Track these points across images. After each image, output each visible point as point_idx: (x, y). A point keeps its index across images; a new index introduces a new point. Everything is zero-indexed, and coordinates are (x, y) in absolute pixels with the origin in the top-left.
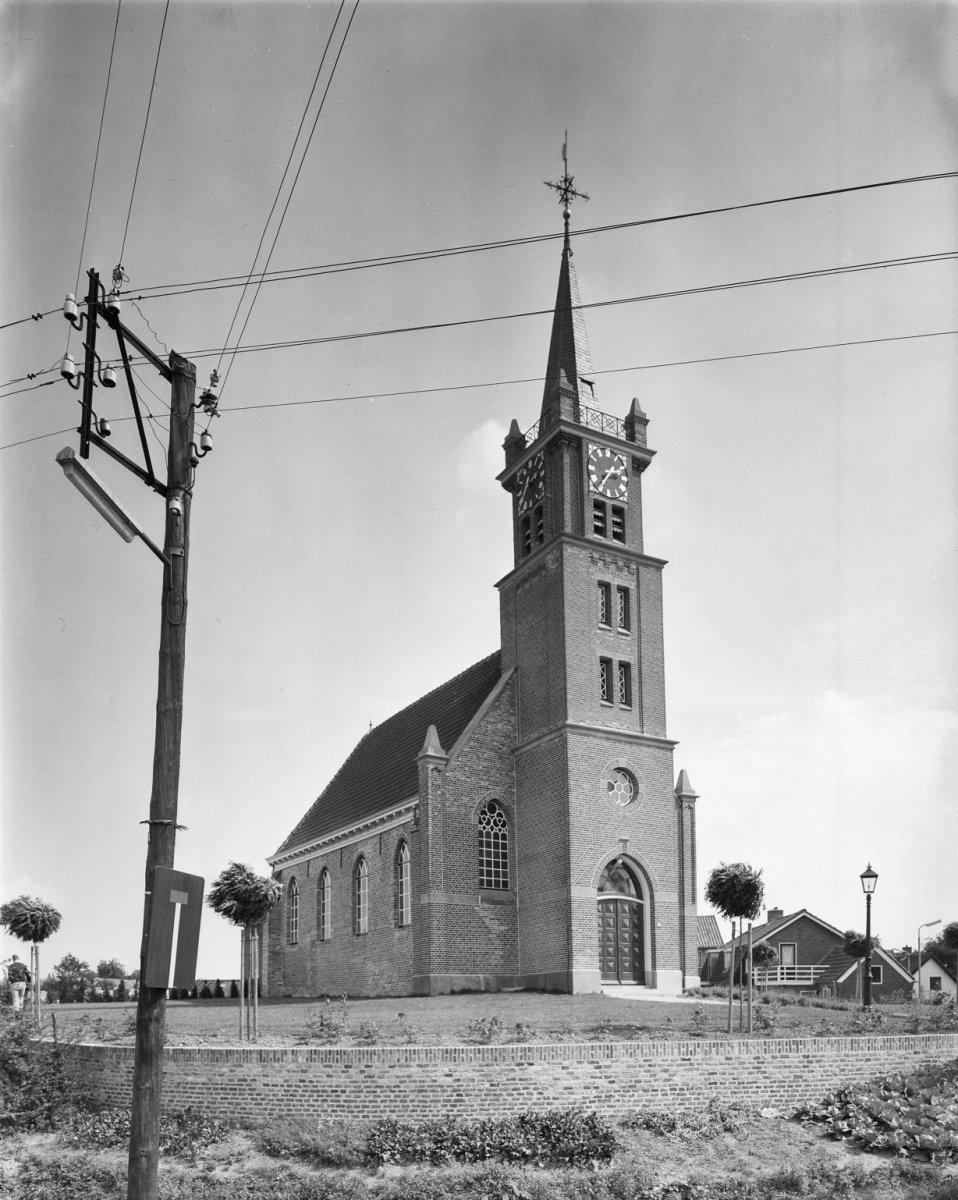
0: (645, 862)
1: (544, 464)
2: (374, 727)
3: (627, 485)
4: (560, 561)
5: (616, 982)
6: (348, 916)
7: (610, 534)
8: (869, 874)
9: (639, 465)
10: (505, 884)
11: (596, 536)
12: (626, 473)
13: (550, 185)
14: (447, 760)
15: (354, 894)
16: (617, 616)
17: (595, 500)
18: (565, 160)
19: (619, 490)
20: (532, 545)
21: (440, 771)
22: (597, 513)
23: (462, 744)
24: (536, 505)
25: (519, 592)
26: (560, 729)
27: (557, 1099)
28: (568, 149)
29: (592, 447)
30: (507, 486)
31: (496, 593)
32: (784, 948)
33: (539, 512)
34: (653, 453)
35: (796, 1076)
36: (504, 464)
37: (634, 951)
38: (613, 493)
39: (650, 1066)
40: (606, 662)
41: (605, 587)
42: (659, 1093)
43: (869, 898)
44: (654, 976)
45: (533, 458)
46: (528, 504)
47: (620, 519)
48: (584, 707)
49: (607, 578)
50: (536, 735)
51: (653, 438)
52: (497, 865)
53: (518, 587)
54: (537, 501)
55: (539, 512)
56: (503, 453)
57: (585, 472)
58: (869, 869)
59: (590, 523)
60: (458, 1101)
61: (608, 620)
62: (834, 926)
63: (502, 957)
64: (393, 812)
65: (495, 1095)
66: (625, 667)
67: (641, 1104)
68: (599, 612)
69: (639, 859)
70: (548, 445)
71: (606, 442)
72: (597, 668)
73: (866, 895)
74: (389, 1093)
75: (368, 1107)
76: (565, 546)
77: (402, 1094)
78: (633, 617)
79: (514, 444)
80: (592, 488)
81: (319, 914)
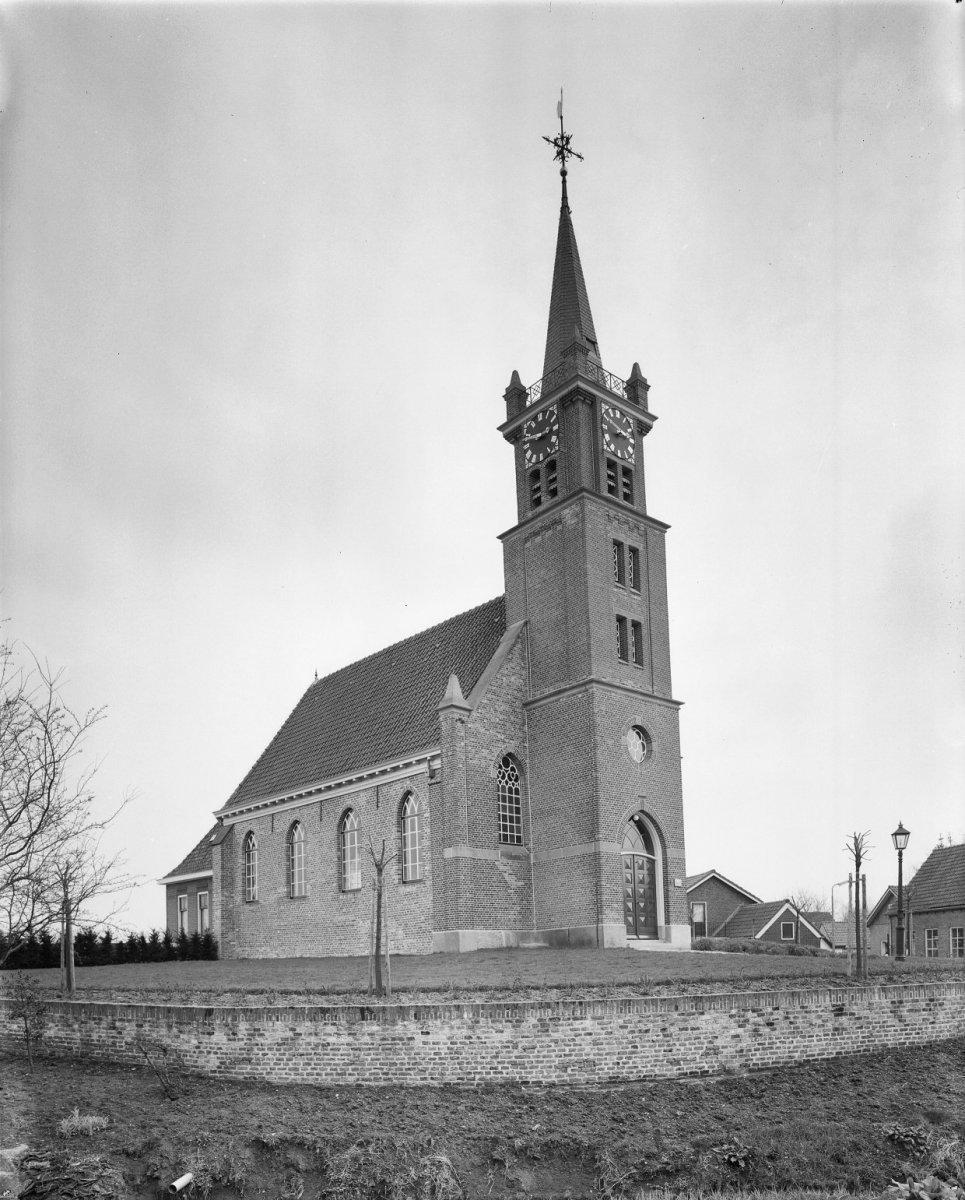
0: (659, 819)
1: (557, 418)
2: (320, 677)
3: (633, 447)
4: (581, 517)
5: (635, 937)
6: (333, 871)
7: (621, 494)
8: (901, 832)
9: (643, 429)
10: (519, 838)
11: (609, 495)
12: (632, 434)
13: (548, 140)
14: (470, 711)
15: (339, 849)
16: (628, 576)
17: (609, 460)
18: (562, 117)
19: (628, 452)
20: (542, 498)
21: (463, 722)
22: (609, 472)
23: (481, 695)
24: (549, 459)
25: (528, 545)
26: (586, 683)
27: (726, 1047)
28: (563, 107)
29: (605, 407)
30: (507, 437)
31: (499, 545)
32: (702, 907)
33: (552, 466)
34: (654, 418)
35: (924, 1020)
36: (505, 415)
37: (626, 906)
38: (622, 454)
39: (806, 1012)
40: (621, 620)
41: (618, 544)
42: (815, 1038)
43: (900, 854)
44: (668, 931)
45: (544, 412)
46: (538, 457)
47: (626, 482)
48: (605, 666)
49: (621, 538)
50: (552, 691)
51: (655, 402)
52: (511, 818)
53: (526, 540)
54: (549, 455)
55: (552, 466)
56: (504, 404)
57: (600, 431)
58: (901, 826)
59: (605, 483)
60: (634, 1053)
61: (621, 580)
62: (749, 891)
63: (520, 913)
64: (413, 760)
65: (669, 1045)
66: (636, 625)
67: (799, 1050)
68: (613, 570)
69: (652, 814)
70: (562, 399)
71: (616, 403)
72: (615, 624)
73: (898, 851)
74: (563, 1047)
75: (542, 1062)
76: (587, 501)
77: (577, 1048)
78: (643, 578)
79: (515, 393)
80: (605, 447)
81: (288, 869)
